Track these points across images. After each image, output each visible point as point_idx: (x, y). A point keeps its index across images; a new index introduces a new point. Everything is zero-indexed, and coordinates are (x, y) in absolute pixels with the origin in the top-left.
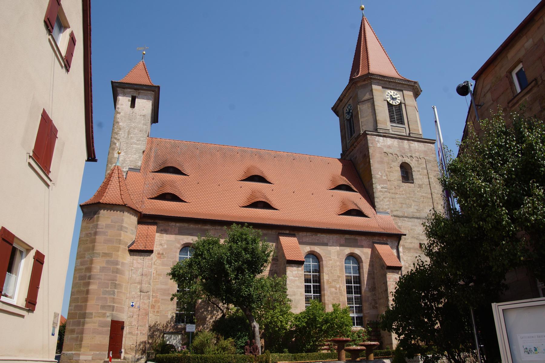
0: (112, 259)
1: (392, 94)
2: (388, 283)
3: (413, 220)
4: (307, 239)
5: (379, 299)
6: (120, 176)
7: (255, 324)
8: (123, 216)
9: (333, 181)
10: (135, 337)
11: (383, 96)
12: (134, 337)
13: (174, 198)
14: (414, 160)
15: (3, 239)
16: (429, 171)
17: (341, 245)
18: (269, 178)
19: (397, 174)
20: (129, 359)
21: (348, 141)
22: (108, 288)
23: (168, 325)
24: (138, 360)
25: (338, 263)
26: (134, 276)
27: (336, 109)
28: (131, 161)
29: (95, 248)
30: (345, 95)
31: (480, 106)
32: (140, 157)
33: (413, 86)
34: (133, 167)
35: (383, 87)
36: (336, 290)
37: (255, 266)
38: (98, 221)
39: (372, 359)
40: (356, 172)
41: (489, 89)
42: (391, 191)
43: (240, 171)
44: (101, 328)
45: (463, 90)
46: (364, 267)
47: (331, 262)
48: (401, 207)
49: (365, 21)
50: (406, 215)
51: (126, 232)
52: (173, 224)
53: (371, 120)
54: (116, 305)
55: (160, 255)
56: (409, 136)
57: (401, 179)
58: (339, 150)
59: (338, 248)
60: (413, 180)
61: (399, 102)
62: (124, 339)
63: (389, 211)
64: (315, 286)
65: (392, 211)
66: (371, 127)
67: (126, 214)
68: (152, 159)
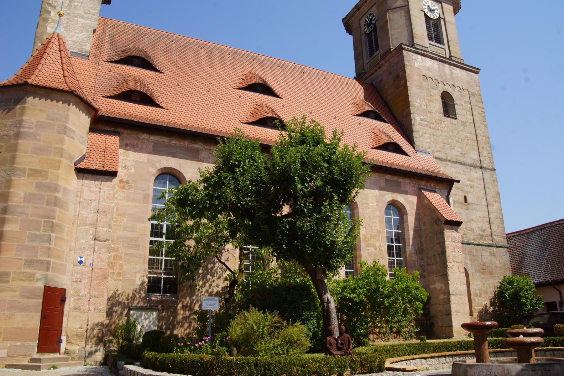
0: (48, 181)
1: (430, 4)
2: (446, 243)
3: (457, 165)
5: (428, 265)
6: (62, 48)
8: (68, 110)
10: (84, 316)
12: (81, 317)
17: (381, 189)
19: (438, 105)
20: (74, 354)
22: (39, 230)
23: (135, 296)
24: (91, 354)
25: (377, 213)
26: (84, 212)
27: (348, 21)
28: (75, 42)
29: (18, 160)
32: (89, 38)
34: (77, 51)
36: (376, 249)
38: (22, 114)
44: (24, 301)
47: (368, 211)
50: (449, 158)
51: (73, 138)
52: (145, 136)
54: (52, 260)
55: (125, 184)
59: (377, 191)
60: (455, 115)
61: (438, 16)
62: (65, 319)
63: (429, 150)
65: (433, 151)
66: (404, 40)
67: (73, 107)
68: (107, 45)
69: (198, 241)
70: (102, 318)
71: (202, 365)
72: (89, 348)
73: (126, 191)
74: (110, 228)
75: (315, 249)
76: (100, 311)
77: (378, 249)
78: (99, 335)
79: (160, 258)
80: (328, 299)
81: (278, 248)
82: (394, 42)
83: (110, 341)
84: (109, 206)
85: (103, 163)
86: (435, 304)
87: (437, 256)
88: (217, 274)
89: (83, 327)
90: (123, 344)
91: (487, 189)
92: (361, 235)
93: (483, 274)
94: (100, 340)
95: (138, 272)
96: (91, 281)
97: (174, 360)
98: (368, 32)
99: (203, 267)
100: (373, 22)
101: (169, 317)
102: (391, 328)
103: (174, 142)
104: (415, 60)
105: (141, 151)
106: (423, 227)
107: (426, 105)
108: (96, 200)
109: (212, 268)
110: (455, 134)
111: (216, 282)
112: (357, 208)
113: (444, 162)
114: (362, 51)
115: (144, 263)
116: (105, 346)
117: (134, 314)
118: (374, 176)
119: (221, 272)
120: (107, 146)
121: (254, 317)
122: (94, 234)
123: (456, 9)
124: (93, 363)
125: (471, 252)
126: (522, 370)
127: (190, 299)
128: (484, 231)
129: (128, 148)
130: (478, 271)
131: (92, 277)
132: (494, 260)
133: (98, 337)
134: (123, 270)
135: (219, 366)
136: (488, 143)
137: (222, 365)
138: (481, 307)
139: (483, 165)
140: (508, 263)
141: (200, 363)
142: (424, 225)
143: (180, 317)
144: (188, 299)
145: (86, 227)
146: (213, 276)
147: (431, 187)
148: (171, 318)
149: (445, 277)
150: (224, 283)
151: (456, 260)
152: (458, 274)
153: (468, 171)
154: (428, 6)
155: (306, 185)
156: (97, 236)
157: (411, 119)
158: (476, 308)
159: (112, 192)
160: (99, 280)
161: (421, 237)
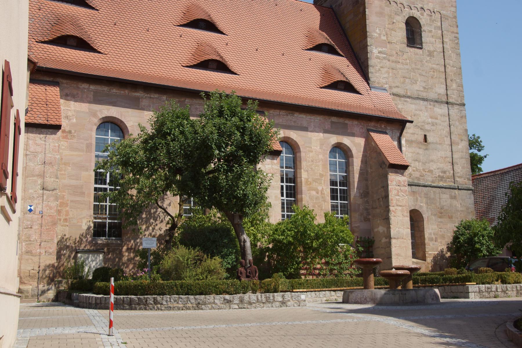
2: (390, 187)
3: (418, 101)
4: (281, 120)
5: (373, 208)
9: (309, 37)
10: (36, 259)
13: (82, 44)
14: (425, 14)
15: (409, 185)
16: (444, 32)
17: (326, 131)
18: (220, 25)
19: (401, 33)
20: (28, 292)
23: (82, 240)
24: (43, 292)
25: (321, 157)
26: (31, 164)
36: (318, 193)
39: (412, 288)
42: (391, 58)
46: (355, 164)
47: (311, 154)
48: (404, 83)
50: (409, 94)
52: (85, 86)
59: (321, 135)
60: (421, 44)
63: (386, 86)
64: (292, 189)
65: (391, 87)
69: (139, 191)
70: (52, 260)
71: (142, 288)
72: (41, 287)
73: (69, 141)
74: (57, 178)
75: (229, 199)
76: (51, 254)
77: (320, 192)
78: (51, 276)
79: (104, 204)
81: (202, 200)
83: (60, 282)
84: (55, 158)
85: (46, 116)
86: (379, 247)
87: (381, 199)
88: (160, 218)
89: (35, 268)
90: (74, 282)
91: (452, 127)
92: (303, 179)
93: (440, 217)
94: (51, 280)
95: (84, 218)
96: (41, 227)
97: (121, 286)
99: (146, 212)
101: (114, 259)
103: (114, 91)
105: (82, 101)
107: (387, 34)
108: (42, 152)
109: (155, 213)
110: (419, 67)
111: (159, 226)
112: (300, 152)
113: (402, 99)
115: (90, 209)
116: (55, 285)
117: (82, 257)
118: (319, 118)
119: (163, 217)
120: (48, 98)
121: (181, 253)
122: (42, 184)
124: (45, 300)
126: (385, 294)
127: (134, 242)
128: (444, 172)
129: (69, 98)
130: (435, 215)
131: (42, 224)
132: (455, 202)
133: (49, 277)
134: (69, 216)
135: (154, 288)
136: (459, 74)
137: (156, 287)
138: (436, 253)
139: (450, 100)
140: (472, 206)
141: (141, 286)
142: (371, 168)
143: (125, 259)
144: (132, 242)
145: (34, 178)
146: (156, 220)
147: (381, 128)
148: (117, 260)
149: (387, 220)
150: (166, 226)
151: (400, 204)
153: (432, 107)
155: (223, 150)
156: (45, 186)
157: (367, 52)
158: (429, 252)
159: (57, 145)
160: (48, 226)
161: (367, 180)
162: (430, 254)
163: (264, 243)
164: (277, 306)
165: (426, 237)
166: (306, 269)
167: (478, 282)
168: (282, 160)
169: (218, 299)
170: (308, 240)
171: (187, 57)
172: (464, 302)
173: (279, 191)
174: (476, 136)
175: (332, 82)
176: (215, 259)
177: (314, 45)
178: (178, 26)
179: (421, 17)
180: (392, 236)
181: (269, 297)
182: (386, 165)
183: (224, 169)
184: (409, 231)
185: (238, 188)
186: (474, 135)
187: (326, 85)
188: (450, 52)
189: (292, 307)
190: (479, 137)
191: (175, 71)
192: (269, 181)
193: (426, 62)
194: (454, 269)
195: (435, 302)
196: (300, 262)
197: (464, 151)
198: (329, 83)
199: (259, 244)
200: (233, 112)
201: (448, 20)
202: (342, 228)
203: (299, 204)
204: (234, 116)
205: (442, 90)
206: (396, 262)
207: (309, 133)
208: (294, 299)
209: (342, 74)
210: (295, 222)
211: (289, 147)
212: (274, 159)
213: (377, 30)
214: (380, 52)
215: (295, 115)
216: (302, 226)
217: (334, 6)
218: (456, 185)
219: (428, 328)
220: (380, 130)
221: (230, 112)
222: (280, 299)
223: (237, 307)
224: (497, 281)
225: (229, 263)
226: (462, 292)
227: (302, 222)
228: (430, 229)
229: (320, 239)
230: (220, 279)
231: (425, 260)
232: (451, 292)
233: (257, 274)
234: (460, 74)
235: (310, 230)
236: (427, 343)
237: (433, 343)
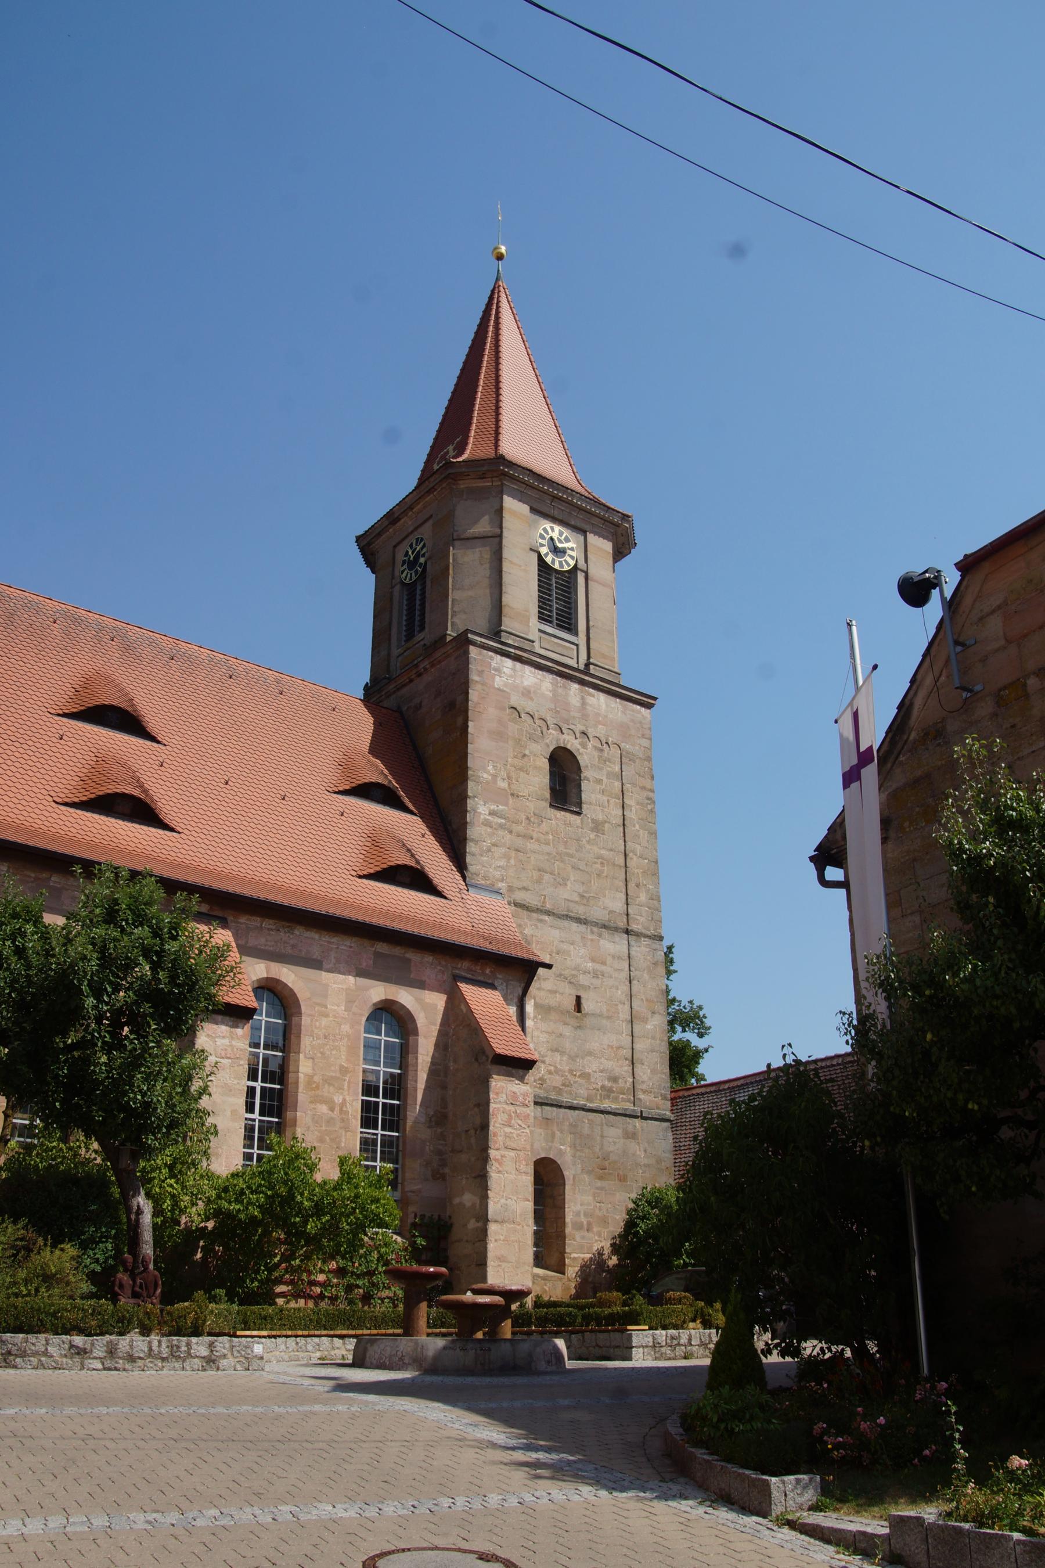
1: (555, 535)
2: (492, 1106)
3: (566, 923)
4: (263, 940)
5: (453, 1151)
7: (141, 1200)
9: (346, 766)
11: (530, 537)
14: (590, 746)
15: (536, 1103)
16: (627, 786)
17: (361, 973)
18: (153, 722)
21: (395, 652)
25: (346, 1028)
27: (369, 544)
30: (411, 508)
31: (962, 644)
33: (617, 525)
35: (533, 510)
36: (332, 1109)
37: (177, 1010)
39: (509, 1336)
40: (418, 749)
41: (999, 607)
42: (517, 828)
43: (59, 680)
45: (915, 590)
46: (420, 1050)
47: (324, 1022)
49: (503, 295)
50: (548, 906)
53: (485, 602)
56: (586, 671)
57: (547, 795)
58: (365, 676)
59: (351, 979)
60: (579, 804)
61: (572, 563)
63: (502, 885)
64: (273, 1095)
65: (511, 889)
66: (480, 622)
77: (337, 1109)
80: (138, 1206)
82: (456, 620)
86: (460, 1241)
87: (472, 1132)
91: (634, 982)
92: (301, 1075)
93: (601, 1178)
98: (408, 581)
100: (422, 560)
102: (349, 1288)
104: (496, 670)
106: (452, 1066)
107: (509, 777)
110: (572, 851)
113: (534, 915)
114: (390, 624)
118: (348, 943)
123: (622, 548)
125: (576, 1126)
126: (445, 1348)
128: (615, 1079)
130: (589, 1172)
132: (633, 1147)
138: (589, 1256)
139: (634, 927)
140: (668, 1157)
142: (455, 1061)
149: (481, 1179)
151: (513, 1145)
152: (512, 1177)
153: (595, 937)
154: (552, 539)
155: (106, 998)
157: (466, 811)
162: (575, 1258)
163: (194, 1215)
164: (196, 1367)
165: (568, 1219)
166: (291, 1282)
167: (654, 1324)
168: (256, 1029)
169: (56, 1345)
170: (297, 1215)
171: (68, 785)
172: (615, 1369)
173: (241, 1101)
174: (696, 1003)
175: (385, 866)
176: (62, 1250)
177: (353, 785)
178: (59, 715)
179: (582, 750)
180: (490, 1217)
181: (178, 1347)
182: (487, 1057)
183: (104, 1043)
184: (530, 1206)
185: (132, 1085)
186: (691, 1002)
187: (372, 871)
188: (637, 827)
189: (232, 1372)
190: (700, 1008)
191: (37, 811)
192: (208, 1076)
193: (588, 842)
194: (615, 1293)
195: (554, 1368)
196: (277, 1266)
197: (658, 1036)
198: (378, 869)
199: (183, 1219)
200: (139, 916)
201: (634, 762)
202: (377, 1194)
203: (288, 1133)
204: (141, 924)
205: (617, 904)
206: (496, 1277)
207: (324, 973)
208: (235, 1353)
209: (409, 850)
210: (270, 1173)
211: (277, 1001)
212: (237, 1027)
213: (490, 768)
214: (492, 813)
215: (297, 932)
216: (285, 1183)
217: (404, 709)
218: (638, 1109)
219: (509, 1430)
220: (481, 978)
221: (134, 913)
222: (204, 1352)
223: (100, 1366)
224: (694, 1320)
225: (97, 1261)
226: (618, 1347)
227: (286, 1174)
228: (578, 1203)
229: (324, 1215)
230: (72, 1297)
231: (563, 1273)
232: (597, 1345)
233: (159, 1291)
234: (655, 874)
235: (302, 1194)
236: (494, 1463)
237: (505, 1464)
